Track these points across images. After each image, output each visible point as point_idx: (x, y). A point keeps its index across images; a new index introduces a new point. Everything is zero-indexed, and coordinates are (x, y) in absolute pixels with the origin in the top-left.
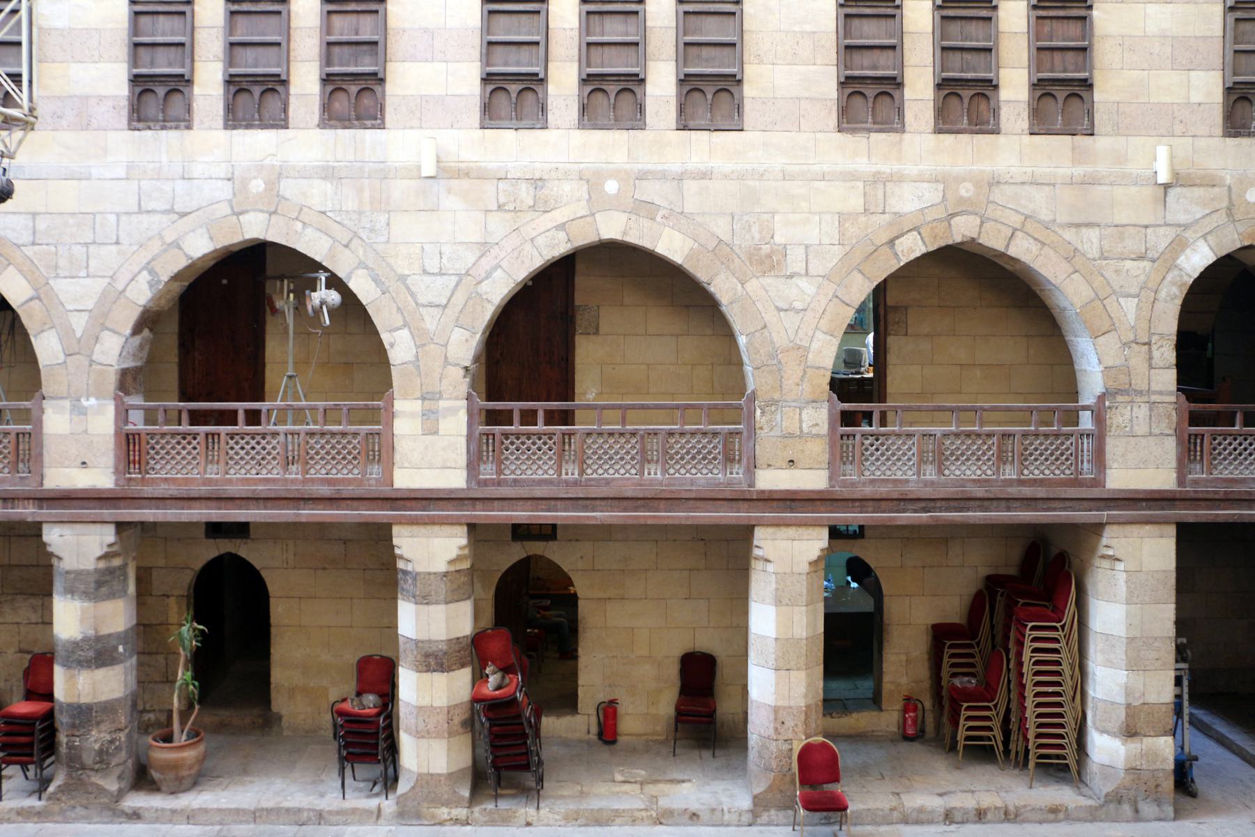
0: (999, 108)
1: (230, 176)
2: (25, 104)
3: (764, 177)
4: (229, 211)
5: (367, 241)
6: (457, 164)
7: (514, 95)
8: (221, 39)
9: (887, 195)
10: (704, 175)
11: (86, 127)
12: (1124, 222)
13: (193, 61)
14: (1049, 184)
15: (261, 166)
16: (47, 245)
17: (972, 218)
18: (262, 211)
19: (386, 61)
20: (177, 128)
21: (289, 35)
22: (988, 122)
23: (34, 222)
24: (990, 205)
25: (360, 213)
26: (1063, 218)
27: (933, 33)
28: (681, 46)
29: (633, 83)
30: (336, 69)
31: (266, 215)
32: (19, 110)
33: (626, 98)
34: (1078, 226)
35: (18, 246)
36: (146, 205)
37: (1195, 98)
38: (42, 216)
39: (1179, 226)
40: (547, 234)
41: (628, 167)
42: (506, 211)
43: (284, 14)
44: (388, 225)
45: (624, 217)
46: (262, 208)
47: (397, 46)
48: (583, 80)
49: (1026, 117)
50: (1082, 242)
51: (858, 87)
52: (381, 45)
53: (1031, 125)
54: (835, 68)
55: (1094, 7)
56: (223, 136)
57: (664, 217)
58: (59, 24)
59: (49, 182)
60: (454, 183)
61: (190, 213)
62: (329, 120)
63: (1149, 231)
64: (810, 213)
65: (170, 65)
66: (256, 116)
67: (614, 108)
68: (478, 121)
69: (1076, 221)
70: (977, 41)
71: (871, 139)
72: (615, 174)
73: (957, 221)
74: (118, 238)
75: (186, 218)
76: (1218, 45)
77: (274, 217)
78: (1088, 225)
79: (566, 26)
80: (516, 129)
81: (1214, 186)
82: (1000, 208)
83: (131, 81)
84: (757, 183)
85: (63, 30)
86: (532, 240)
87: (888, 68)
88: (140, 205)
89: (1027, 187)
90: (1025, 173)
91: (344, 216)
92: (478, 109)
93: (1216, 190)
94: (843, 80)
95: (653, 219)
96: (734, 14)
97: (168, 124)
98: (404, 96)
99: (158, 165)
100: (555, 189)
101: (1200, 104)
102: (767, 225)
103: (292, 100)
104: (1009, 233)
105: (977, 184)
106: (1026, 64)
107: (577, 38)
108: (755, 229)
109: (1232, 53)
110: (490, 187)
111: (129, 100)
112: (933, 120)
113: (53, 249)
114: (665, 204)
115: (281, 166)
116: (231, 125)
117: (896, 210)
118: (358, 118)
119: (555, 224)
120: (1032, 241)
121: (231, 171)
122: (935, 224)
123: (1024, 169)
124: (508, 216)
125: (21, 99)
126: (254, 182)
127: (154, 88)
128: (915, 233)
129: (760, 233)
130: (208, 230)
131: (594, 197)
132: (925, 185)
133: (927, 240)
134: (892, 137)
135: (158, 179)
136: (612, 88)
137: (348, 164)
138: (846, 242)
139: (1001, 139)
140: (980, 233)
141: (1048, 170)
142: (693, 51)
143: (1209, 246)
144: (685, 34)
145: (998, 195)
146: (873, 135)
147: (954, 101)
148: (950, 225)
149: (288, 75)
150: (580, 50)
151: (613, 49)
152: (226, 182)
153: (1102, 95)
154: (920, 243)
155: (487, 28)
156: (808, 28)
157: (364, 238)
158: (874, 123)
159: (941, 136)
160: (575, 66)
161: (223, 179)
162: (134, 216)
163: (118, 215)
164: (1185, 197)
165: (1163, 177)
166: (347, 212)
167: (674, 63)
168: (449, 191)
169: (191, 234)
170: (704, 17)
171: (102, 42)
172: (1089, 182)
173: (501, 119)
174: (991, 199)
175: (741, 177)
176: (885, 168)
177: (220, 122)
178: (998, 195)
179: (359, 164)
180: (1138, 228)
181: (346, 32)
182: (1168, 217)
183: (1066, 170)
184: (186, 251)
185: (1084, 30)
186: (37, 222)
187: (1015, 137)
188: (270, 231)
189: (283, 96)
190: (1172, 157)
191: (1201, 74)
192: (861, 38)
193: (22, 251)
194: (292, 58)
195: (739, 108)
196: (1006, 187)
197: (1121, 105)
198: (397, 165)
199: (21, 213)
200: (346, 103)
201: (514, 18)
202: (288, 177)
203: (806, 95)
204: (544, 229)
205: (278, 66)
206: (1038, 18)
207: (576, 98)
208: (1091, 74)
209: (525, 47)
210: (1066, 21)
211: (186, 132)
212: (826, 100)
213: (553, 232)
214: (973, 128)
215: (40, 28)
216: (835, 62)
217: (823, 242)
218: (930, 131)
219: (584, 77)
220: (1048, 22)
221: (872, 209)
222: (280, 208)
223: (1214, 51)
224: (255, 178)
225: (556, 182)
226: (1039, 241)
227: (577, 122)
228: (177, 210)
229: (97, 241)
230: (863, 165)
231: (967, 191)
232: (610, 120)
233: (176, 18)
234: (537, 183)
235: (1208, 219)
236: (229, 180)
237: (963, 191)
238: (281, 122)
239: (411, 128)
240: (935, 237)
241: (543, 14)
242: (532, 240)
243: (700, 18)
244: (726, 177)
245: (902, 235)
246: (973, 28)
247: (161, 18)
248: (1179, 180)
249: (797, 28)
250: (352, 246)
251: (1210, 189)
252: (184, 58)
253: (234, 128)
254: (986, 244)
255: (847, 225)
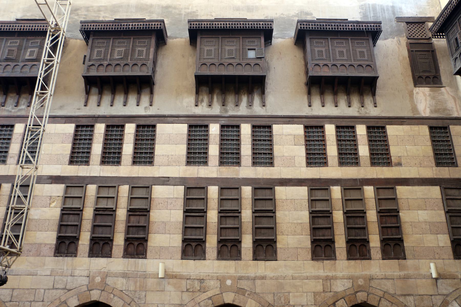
0: (370, 250)
1: (88, 275)
2: (19, 247)
3: (285, 279)
4: (86, 289)
5: (137, 303)
6: (172, 273)
7: (194, 247)
8: (91, 223)
9: (331, 284)
10: (263, 278)
11: (39, 255)
12: (423, 293)
13: (80, 231)
14: (391, 279)
15: (100, 272)
16: (16, 302)
17: (364, 293)
18: (99, 290)
19: (148, 233)
20: (71, 256)
21: (115, 223)
22: (366, 255)
23: (13, 292)
24: (370, 288)
25: (135, 291)
26: (398, 292)
27: (344, 222)
28: (254, 229)
29: (237, 243)
30: (131, 236)
31: (100, 291)
32: (16, 250)
33: (234, 249)
34: (405, 295)
35: (4, 302)
36: (56, 286)
37: (441, 244)
38: (16, 290)
39: (444, 295)
40: (205, 301)
41: (235, 275)
42: (189, 292)
43: (114, 215)
44: (145, 296)
45: (233, 294)
46: (99, 288)
47: (153, 228)
48: (219, 241)
49: (380, 253)
50: (407, 302)
51: (318, 243)
52: (147, 227)
53: (382, 256)
54: (309, 236)
55: (400, 211)
56: (87, 260)
57: (248, 294)
58: (36, 218)
59: (22, 276)
60: (171, 280)
61: (72, 290)
62: (126, 255)
63: (433, 297)
64: (303, 292)
65: (72, 233)
66: (100, 253)
67: (230, 252)
68: (180, 256)
69: (404, 293)
70: (360, 225)
71: (324, 263)
72: (230, 278)
73: (359, 294)
74: (43, 299)
75: (70, 292)
76: (445, 225)
77: (103, 292)
78: (409, 295)
79: (213, 221)
80: (194, 260)
81: (454, 279)
82: (374, 289)
83: (57, 238)
84: (283, 281)
85: (37, 219)
86: (199, 303)
87: (329, 236)
88: (54, 286)
89: (384, 280)
90: (382, 275)
91: (129, 292)
92: (180, 252)
93: (456, 280)
94: (312, 240)
95: (244, 295)
96: (273, 217)
97: (68, 255)
98: (154, 247)
99: (62, 270)
100: (208, 283)
101: (443, 247)
102: (287, 298)
103: (114, 247)
104: (379, 299)
105: (365, 279)
106: (378, 233)
107: (217, 226)
108: (282, 299)
109: (451, 228)
110: (184, 282)
111: (55, 245)
112: (346, 255)
113: (18, 303)
114: (248, 289)
115: (107, 272)
116: (91, 256)
117: (335, 291)
118: (137, 255)
119: (208, 297)
120: (388, 302)
121: (89, 273)
122: (350, 296)
123: (382, 273)
124: (190, 294)
125: (17, 245)
126: (97, 278)
127: (65, 241)
128: (343, 300)
129: (284, 301)
130: (78, 297)
131: (222, 286)
132: (345, 280)
133: (347, 302)
134: (332, 262)
135: (62, 276)
136: (229, 245)
137: (132, 272)
138: (317, 304)
139: (372, 262)
140: (367, 299)
141: (390, 273)
142: (258, 231)
143: (458, 304)
144: (255, 224)
145: (373, 284)
146: (325, 261)
147: (354, 248)
148: (356, 296)
149: (113, 237)
150: (218, 230)
151: (230, 230)
152: (87, 278)
153: (407, 244)
154: (345, 303)
155: (185, 221)
156: (299, 221)
157: (136, 301)
158: (325, 257)
159: (350, 261)
160: (216, 236)
161: (86, 276)
162: (51, 290)
163: (45, 290)
164: (444, 283)
165: (434, 275)
166: (130, 291)
167: (251, 235)
168: (169, 283)
169: (71, 298)
170: (262, 218)
171: (50, 224)
172: (406, 278)
173: (188, 256)
174: (370, 285)
175: (277, 279)
176: (330, 274)
177: (87, 255)
178: (373, 284)
179: (136, 272)
180: (428, 296)
181: (135, 222)
182: (439, 292)
183: (397, 273)
184: (68, 305)
185: (397, 220)
186: (14, 292)
187: (377, 261)
188: (101, 298)
189: (111, 246)
190: (436, 267)
191: (441, 235)
192: (318, 225)
193: (5, 304)
194: (115, 231)
195: (276, 252)
196: (376, 281)
197: (414, 248)
198: (150, 273)
199: (8, 289)
200: (133, 249)
201: (195, 218)
202: (109, 276)
203: (300, 246)
204: (204, 299)
205: (110, 234)
206: (381, 216)
207: (216, 248)
208: (402, 236)
209: (198, 229)
210: (390, 217)
211: (74, 258)
212: (307, 248)
213: (207, 300)
214: (361, 257)
215: (29, 219)
216: (309, 234)
217: (308, 304)
218: (346, 259)
219: (219, 240)
220: (384, 217)
221: (326, 290)
222: (105, 288)
223: (444, 227)
224: (97, 276)
225: (208, 281)
226: (391, 302)
227: (216, 257)
228: (67, 288)
229: (35, 300)
230: (322, 273)
231: (361, 282)
232: (228, 257)
233: (76, 216)
234: (201, 281)
235: (455, 293)
236: (88, 277)
237: (360, 282)
238: (109, 255)
239: (156, 259)
240: (351, 301)
241: (205, 217)
242: (199, 303)
243: (261, 218)
244: (271, 278)
245: (338, 301)
246: (358, 220)
247: (71, 216)
248: (440, 276)
249: (295, 222)
250: (131, 304)
251: (453, 280)
252: (77, 230)
253: (92, 257)
254: (370, 304)
255: (317, 297)
